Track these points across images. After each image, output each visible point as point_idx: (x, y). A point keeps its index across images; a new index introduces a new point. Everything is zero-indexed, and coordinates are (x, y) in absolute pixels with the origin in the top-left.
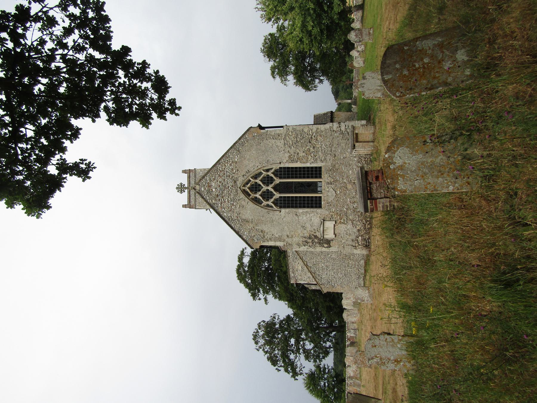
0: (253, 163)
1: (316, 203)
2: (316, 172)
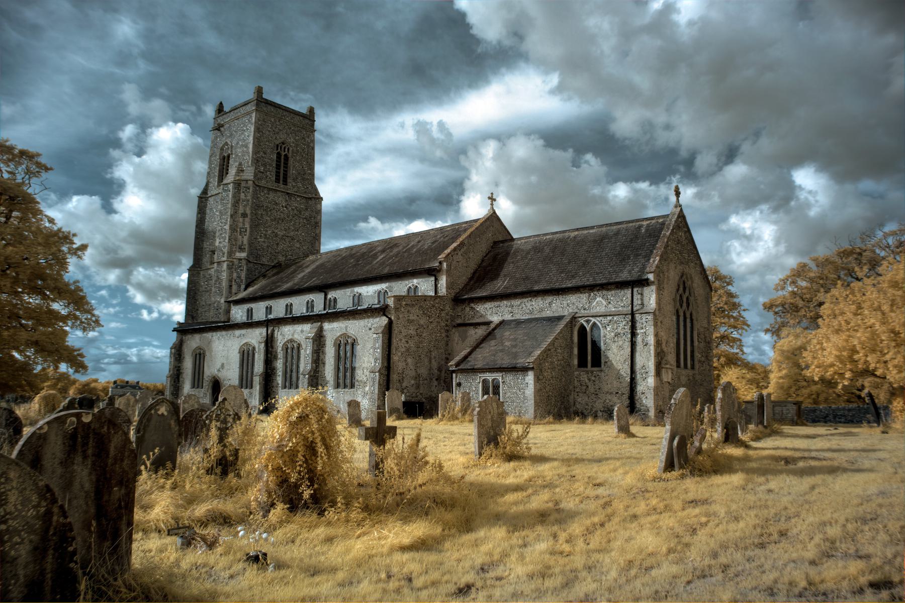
0: (697, 283)
1: (678, 366)
2: (693, 367)
